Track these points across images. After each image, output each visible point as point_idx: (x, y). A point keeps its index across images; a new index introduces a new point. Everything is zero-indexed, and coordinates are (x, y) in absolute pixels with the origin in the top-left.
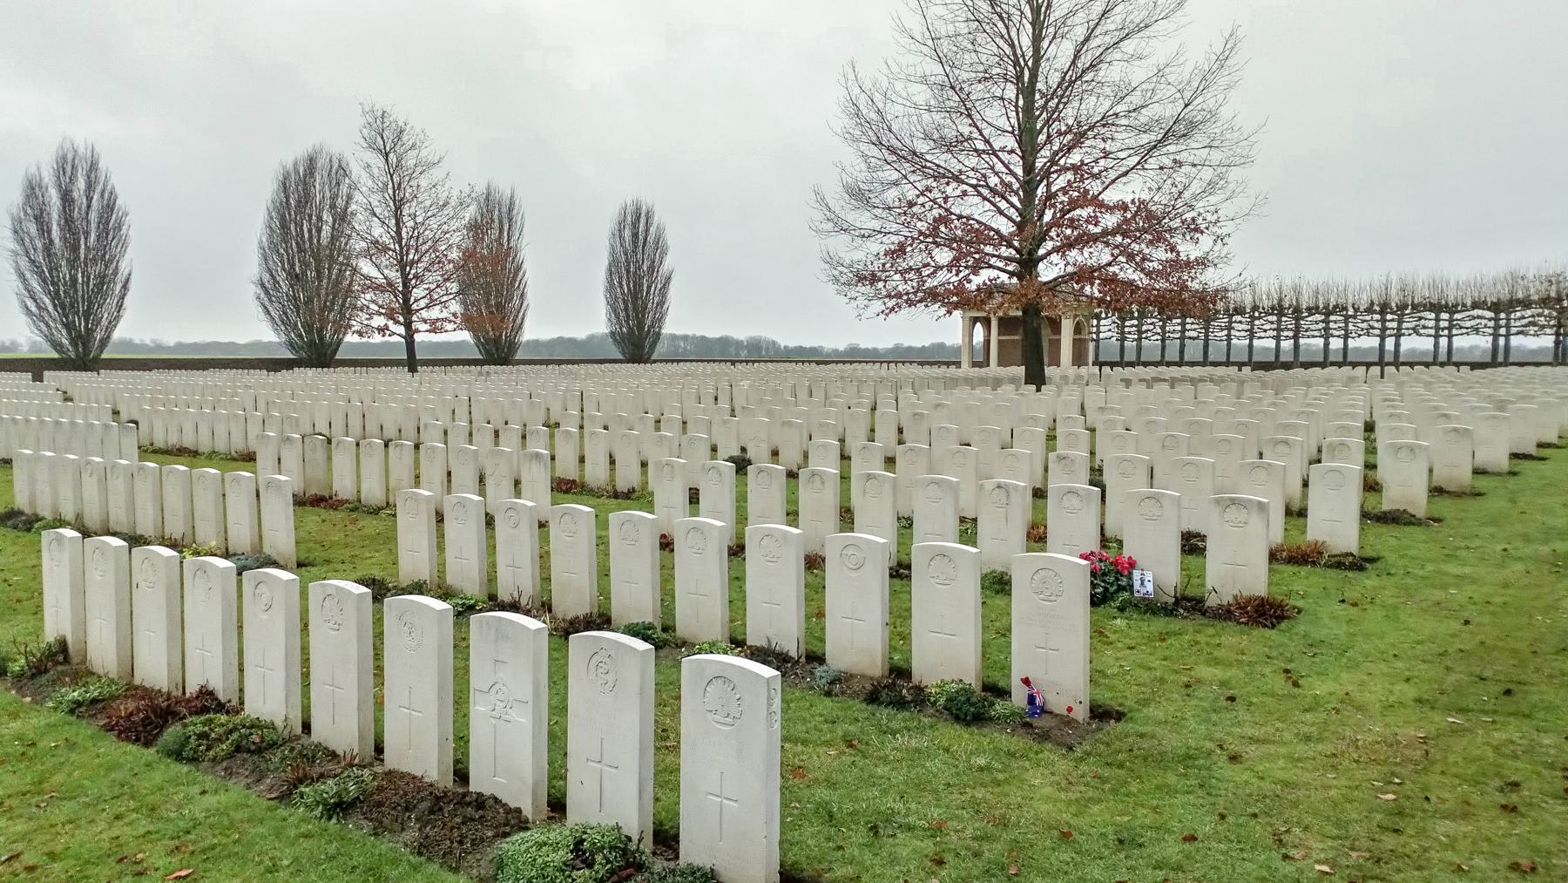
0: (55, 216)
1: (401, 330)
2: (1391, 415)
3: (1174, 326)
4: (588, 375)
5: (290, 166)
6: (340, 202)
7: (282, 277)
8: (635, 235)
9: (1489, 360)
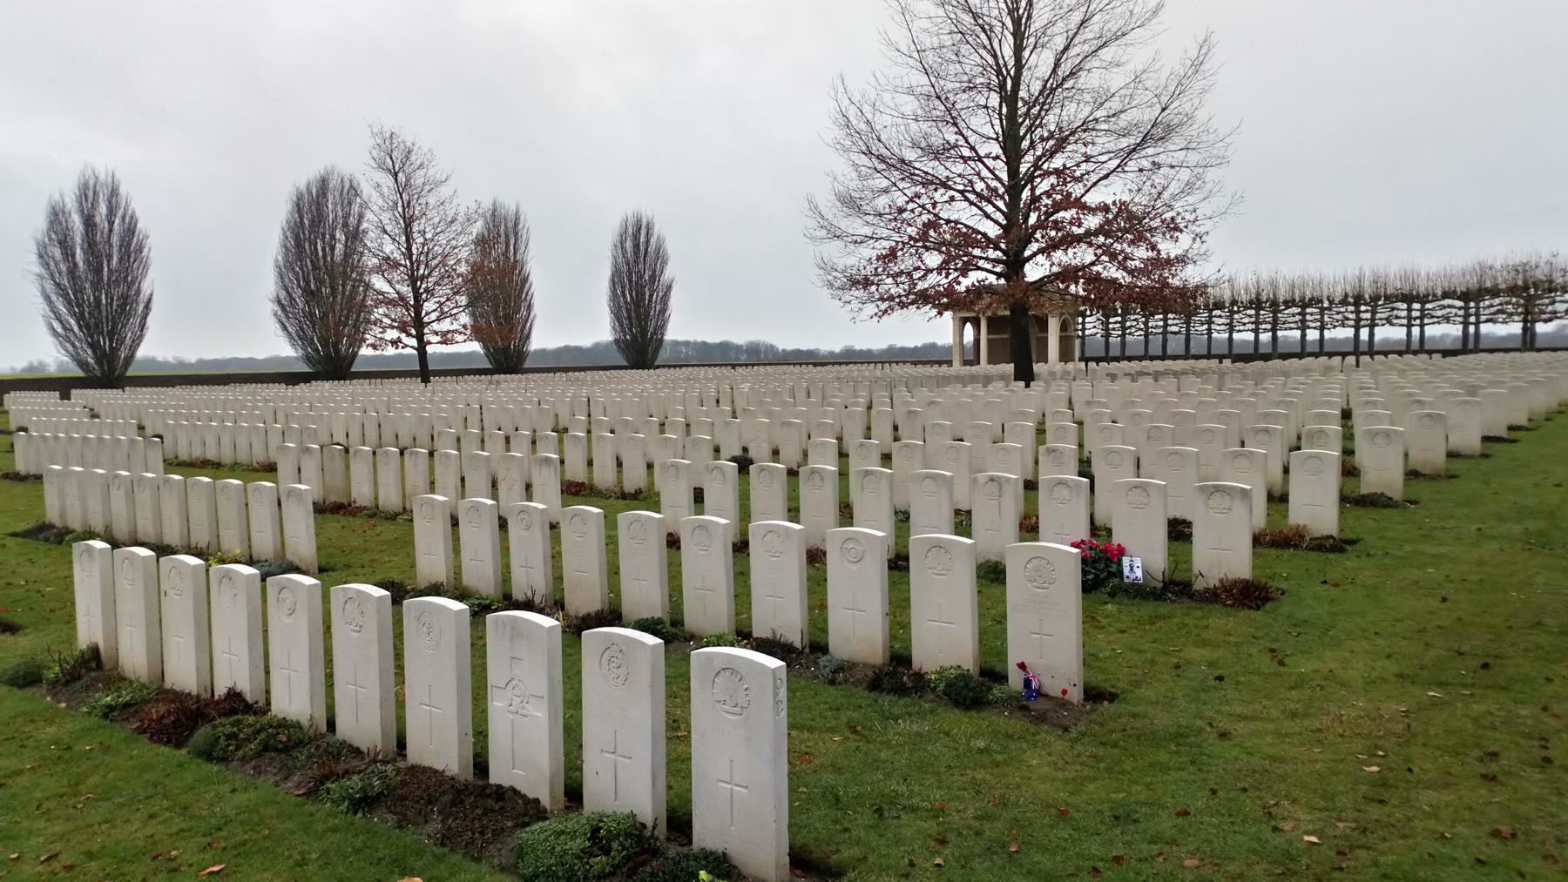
1: (414, 342)
2: (1367, 403)
5: (303, 187)
8: (636, 246)
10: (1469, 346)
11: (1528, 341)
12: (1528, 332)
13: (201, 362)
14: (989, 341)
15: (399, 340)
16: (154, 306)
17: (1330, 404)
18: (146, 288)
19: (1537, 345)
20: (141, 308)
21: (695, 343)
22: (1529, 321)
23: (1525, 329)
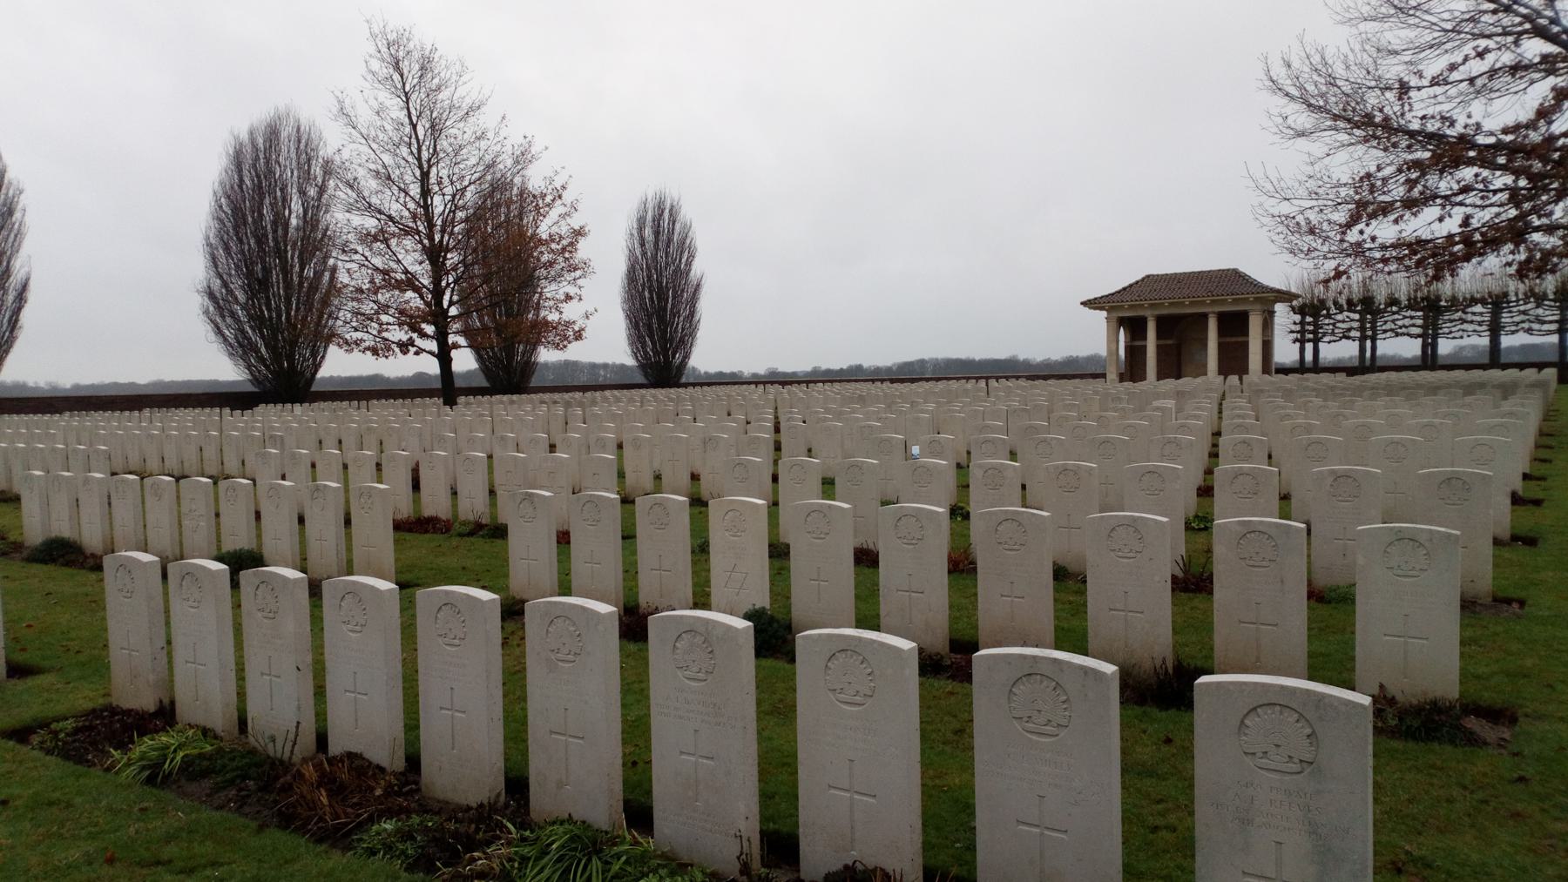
0: (295, 198)
1: (433, 346)
2: (1240, 426)
3: (1420, 322)
4: (643, 397)
5: (245, 137)
6: (1269, 187)
7: (236, 284)
8: (657, 233)
9: (1486, 361)
10: (1366, 366)
11: (1429, 361)
12: (1429, 347)
13: (77, 387)
14: (1158, 347)
15: (411, 342)
16: (32, 296)
17: (765, 420)
18: (19, 267)
19: (1503, 360)
20: (11, 297)
21: (614, 365)
22: (1429, 338)
23: (1434, 346)
